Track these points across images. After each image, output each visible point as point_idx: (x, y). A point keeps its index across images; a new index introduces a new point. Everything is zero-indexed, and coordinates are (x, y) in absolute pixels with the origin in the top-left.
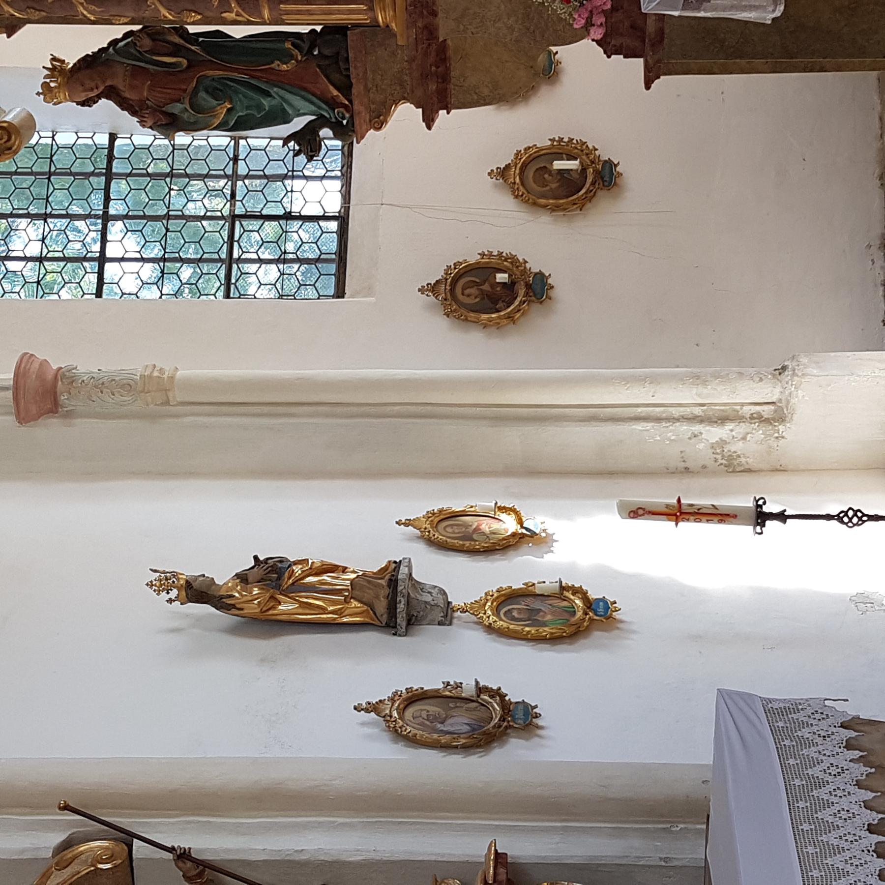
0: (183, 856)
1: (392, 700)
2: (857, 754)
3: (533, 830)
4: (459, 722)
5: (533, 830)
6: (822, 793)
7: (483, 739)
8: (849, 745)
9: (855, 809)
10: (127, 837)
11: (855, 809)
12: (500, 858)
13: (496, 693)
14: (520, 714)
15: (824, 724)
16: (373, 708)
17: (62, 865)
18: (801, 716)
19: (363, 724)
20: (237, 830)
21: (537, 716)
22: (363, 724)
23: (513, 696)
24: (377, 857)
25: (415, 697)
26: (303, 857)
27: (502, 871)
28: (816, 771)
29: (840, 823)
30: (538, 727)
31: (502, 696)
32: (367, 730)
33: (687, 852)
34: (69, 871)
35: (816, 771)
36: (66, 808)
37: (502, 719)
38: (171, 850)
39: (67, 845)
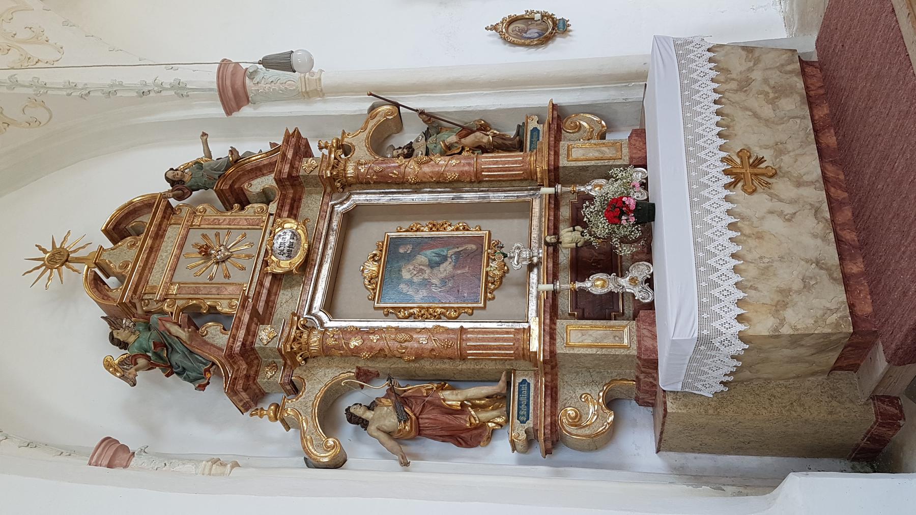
0: (422, 113)
1: (502, 23)
2: (713, 64)
3: (568, 90)
4: (533, 32)
5: (568, 90)
6: (696, 86)
7: (544, 39)
8: (711, 60)
9: (709, 93)
10: (398, 106)
11: (709, 93)
12: (554, 106)
13: (551, 17)
14: (561, 25)
15: (700, 51)
16: (494, 28)
17: (372, 118)
18: (690, 47)
19: (490, 35)
20: (442, 99)
21: (569, 25)
22: (490, 35)
23: (558, 16)
24: (502, 107)
25: (513, 20)
26: (470, 109)
27: (555, 113)
28: (694, 76)
29: (707, 146)
30: (570, 31)
31: (553, 19)
32: (491, 39)
33: (635, 94)
34: (375, 120)
35: (694, 76)
36: (371, 94)
37: (553, 29)
38: (417, 111)
39: (373, 108)
